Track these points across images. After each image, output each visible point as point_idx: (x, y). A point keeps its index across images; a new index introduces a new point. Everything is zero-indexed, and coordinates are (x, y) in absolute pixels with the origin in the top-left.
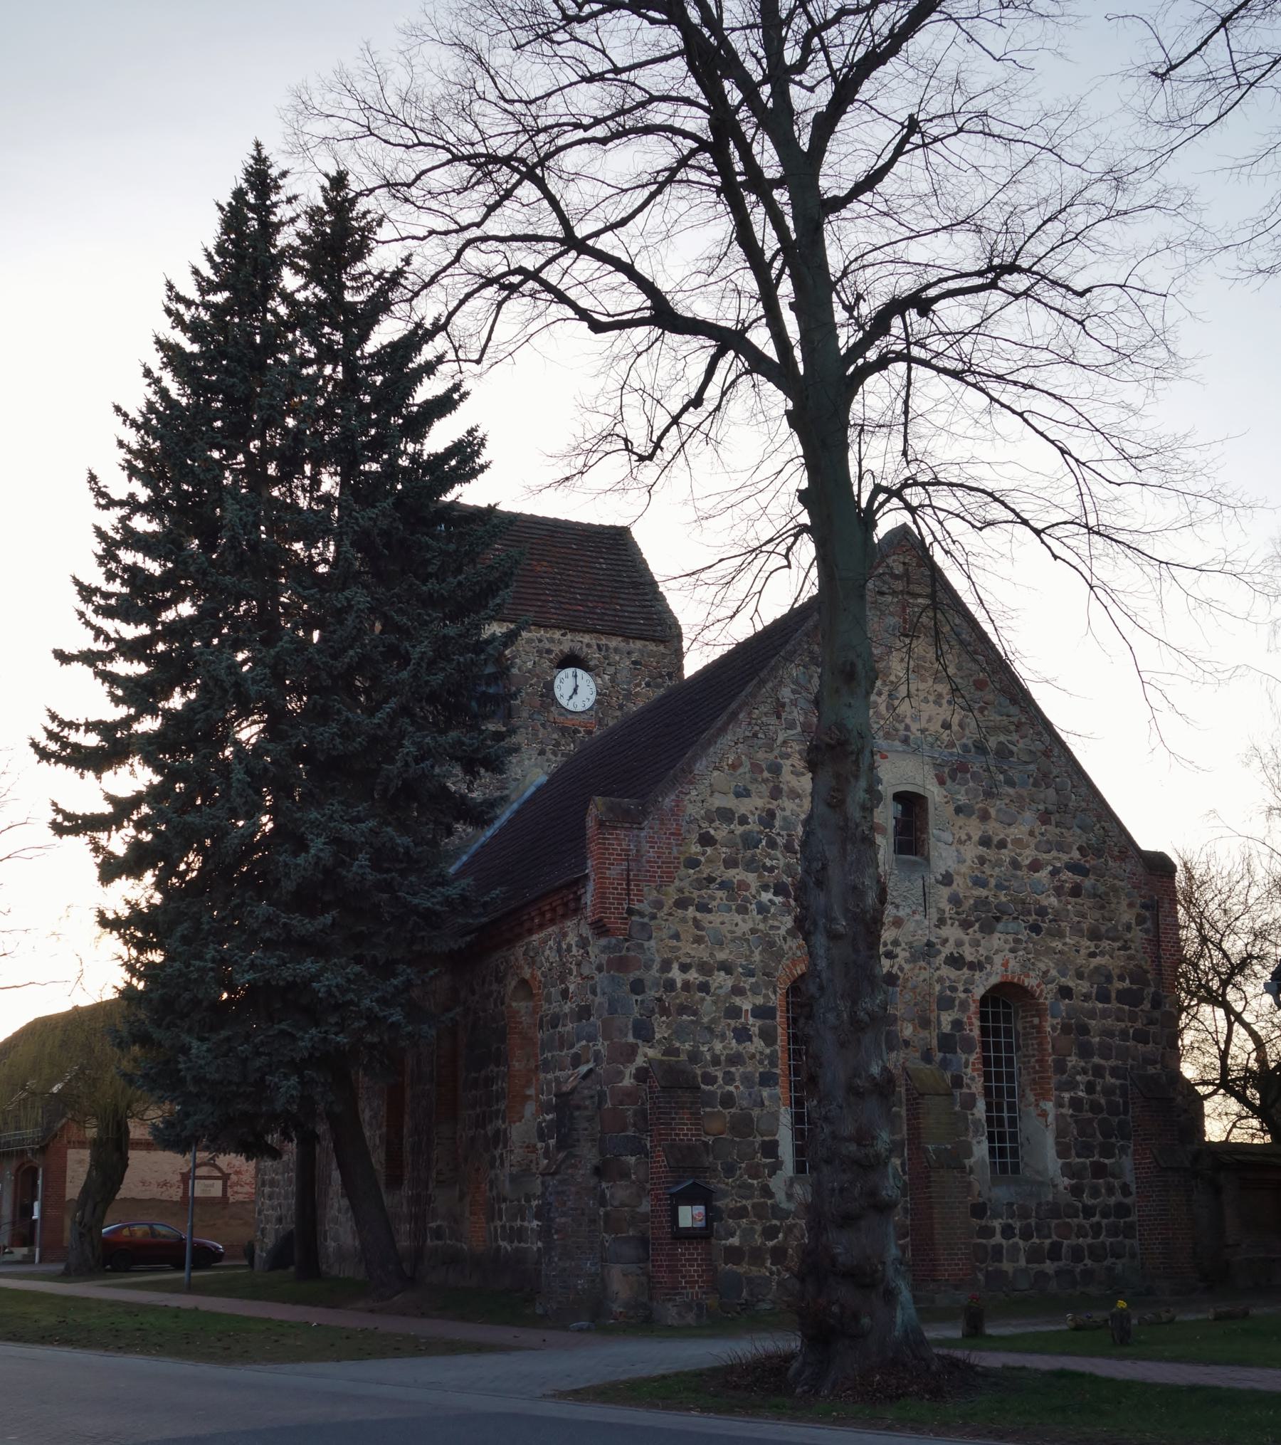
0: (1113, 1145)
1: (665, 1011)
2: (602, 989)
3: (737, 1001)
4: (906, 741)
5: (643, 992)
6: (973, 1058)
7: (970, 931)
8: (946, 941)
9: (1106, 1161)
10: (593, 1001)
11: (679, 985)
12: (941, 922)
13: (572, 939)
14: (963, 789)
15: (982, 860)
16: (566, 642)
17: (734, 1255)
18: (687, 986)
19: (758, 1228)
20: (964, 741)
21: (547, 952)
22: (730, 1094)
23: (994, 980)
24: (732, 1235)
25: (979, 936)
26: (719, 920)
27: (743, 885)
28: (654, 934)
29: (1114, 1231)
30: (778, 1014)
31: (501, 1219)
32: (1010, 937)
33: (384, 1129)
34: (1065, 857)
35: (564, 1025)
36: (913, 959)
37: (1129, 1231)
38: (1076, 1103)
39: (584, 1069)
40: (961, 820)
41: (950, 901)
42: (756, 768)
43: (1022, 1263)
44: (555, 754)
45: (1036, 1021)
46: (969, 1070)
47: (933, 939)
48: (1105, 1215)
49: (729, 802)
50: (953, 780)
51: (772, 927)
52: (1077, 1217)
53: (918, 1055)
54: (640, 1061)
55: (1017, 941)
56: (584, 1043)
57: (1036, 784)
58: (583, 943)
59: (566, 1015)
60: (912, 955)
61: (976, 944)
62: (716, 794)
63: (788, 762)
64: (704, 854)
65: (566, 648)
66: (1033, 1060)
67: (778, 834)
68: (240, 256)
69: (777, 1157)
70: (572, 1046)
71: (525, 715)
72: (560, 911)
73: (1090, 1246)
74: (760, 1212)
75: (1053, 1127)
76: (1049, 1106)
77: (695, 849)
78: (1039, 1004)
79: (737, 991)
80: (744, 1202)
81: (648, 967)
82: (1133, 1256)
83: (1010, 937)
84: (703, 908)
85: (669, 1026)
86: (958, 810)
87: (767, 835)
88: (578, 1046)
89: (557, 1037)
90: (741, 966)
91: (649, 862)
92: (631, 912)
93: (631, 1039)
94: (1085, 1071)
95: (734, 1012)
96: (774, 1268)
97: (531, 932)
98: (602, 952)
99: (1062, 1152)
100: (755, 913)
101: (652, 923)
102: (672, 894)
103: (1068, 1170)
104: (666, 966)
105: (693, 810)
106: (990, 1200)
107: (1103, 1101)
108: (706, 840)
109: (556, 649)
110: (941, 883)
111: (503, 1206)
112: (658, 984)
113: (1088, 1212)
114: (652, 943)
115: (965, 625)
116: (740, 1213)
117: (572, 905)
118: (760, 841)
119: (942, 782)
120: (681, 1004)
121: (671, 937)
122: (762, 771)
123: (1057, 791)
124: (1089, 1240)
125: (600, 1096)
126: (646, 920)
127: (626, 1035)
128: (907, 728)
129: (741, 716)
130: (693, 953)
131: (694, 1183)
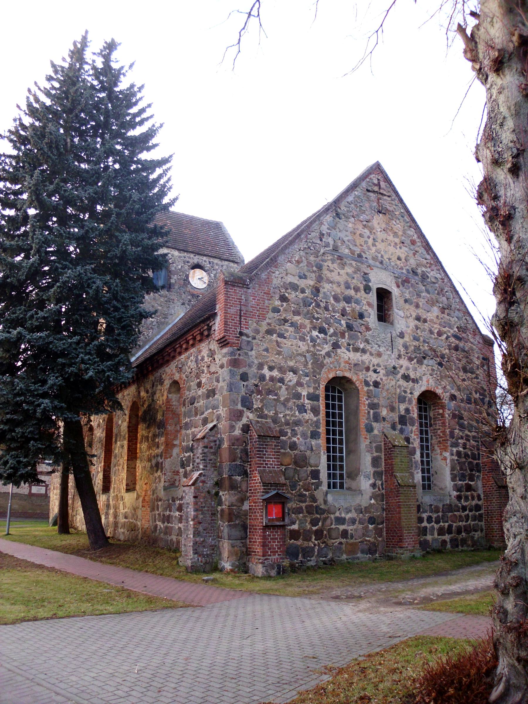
0: (474, 475)
1: (259, 392)
2: (223, 378)
3: (299, 389)
4: (381, 263)
5: (247, 380)
6: (414, 428)
7: (413, 362)
8: (402, 366)
9: (471, 483)
10: (217, 386)
11: (268, 378)
12: (400, 356)
13: (205, 353)
14: (407, 291)
15: (417, 328)
16: (196, 259)
17: (294, 535)
18: (272, 379)
19: (309, 520)
20: (407, 267)
21: (189, 363)
22: (295, 443)
23: (423, 389)
24: (294, 523)
25: (417, 366)
26: (290, 343)
27: (303, 326)
28: (254, 348)
29: (474, 518)
30: (321, 398)
31: (158, 510)
32: (430, 368)
33: (103, 464)
34: (452, 331)
35: (198, 402)
36: (387, 374)
37: (480, 518)
38: (459, 454)
39: (210, 425)
40: (407, 306)
41: (403, 346)
42: (309, 264)
43: (436, 535)
44: (189, 305)
45: (441, 411)
46: (413, 435)
47: (397, 366)
48: (471, 510)
49: (295, 280)
50: (403, 286)
51: (318, 350)
52: (459, 511)
53: (389, 426)
54: (244, 420)
55: (433, 370)
56: (210, 410)
57: (438, 294)
58: (212, 354)
59: (199, 396)
60: (386, 373)
61: (415, 369)
62: (289, 275)
63: (326, 264)
64: (282, 306)
65: (196, 261)
66: (439, 431)
67: (321, 301)
68: (79, 172)
69: (319, 479)
70: (203, 413)
71: (176, 287)
72: (198, 338)
73: (464, 526)
74: (310, 510)
75: (449, 465)
76: (447, 454)
77: (278, 303)
78: (442, 403)
79: (299, 384)
80: (301, 504)
81: (250, 366)
82: (482, 531)
83: (430, 368)
84: (281, 336)
85: (262, 401)
86: (406, 301)
87: (315, 301)
88: (206, 413)
89: (193, 410)
90: (302, 370)
91: (252, 307)
92: (241, 334)
93: (239, 407)
94: (462, 438)
95: (298, 396)
96: (316, 542)
97: (180, 354)
98: (224, 357)
99: (453, 479)
100: (309, 341)
101: (254, 341)
102: (264, 327)
103: (458, 489)
104: (261, 366)
105: (276, 282)
106: (422, 503)
107: (469, 453)
108: (283, 299)
109: (191, 261)
110: (399, 336)
111: (160, 503)
112: (256, 376)
113: (464, 508)
114: (253, 352)
115: (406, 213)
116: (299, 511)
117: (206, 333)
118: (312, 303)
119: (398, 286)
120: (269, 389)
121: (264, 350)
122: (313, 267)
123: (447, 299)
124: (464, 523)
125: (219, 441)
126: (250, 339)
127: (237, 405)
128: (382, 256)
129: (302, 236)
130: (276, 360)
131: (277, 493)
